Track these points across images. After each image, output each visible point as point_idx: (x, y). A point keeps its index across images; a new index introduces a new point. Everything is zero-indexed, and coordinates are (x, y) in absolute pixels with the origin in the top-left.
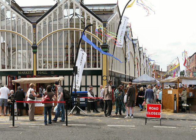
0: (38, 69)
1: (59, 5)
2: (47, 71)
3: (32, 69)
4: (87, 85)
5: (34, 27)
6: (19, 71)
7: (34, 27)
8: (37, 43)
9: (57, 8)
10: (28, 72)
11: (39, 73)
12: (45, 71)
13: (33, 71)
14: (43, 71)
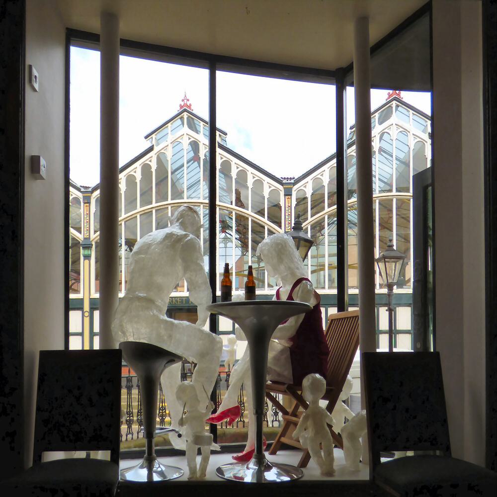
1: (156, 149)
5: (288, 194)
7: (288, 194)
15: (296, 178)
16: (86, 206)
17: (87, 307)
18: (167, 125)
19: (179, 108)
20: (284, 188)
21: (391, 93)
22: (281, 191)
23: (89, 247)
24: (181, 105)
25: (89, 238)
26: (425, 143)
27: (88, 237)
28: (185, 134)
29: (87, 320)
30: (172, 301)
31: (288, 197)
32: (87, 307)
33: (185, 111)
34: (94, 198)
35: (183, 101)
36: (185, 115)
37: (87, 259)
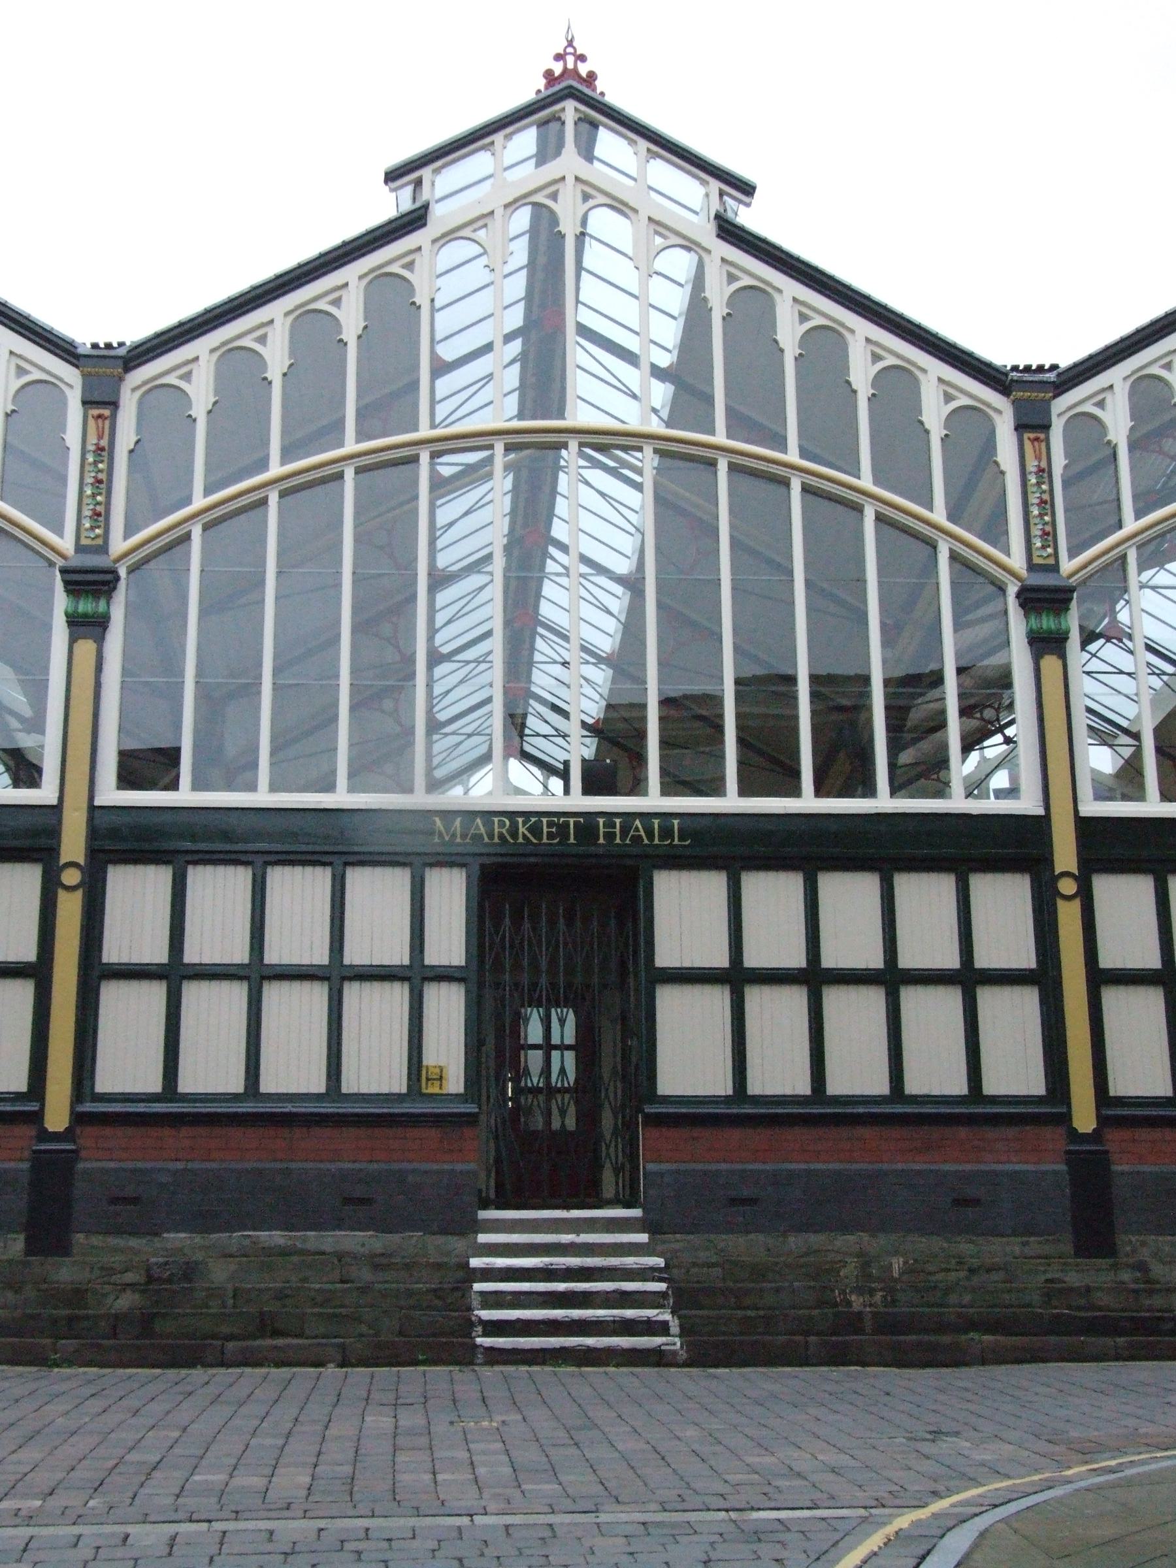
3: (45, 794)
4: (978, 964)
10: (488, 824)
11: (610, 836)
15: (128, 344)
17: (1065, 856)
19: (541, 83)
20: (83, 375)
21: (557, 73)
22: (71, 386)
23: (104, 583)
24: (549, 74)
25: (103, 549)
26: (704, 255)
27: (100, 542)
28: (570, 180)
29: (70, 908)
30: (514, 832)
31: (96, 412)
32: (1065, 856)
33: (571, 94)
34: (134, 390)
35: (559, 57)
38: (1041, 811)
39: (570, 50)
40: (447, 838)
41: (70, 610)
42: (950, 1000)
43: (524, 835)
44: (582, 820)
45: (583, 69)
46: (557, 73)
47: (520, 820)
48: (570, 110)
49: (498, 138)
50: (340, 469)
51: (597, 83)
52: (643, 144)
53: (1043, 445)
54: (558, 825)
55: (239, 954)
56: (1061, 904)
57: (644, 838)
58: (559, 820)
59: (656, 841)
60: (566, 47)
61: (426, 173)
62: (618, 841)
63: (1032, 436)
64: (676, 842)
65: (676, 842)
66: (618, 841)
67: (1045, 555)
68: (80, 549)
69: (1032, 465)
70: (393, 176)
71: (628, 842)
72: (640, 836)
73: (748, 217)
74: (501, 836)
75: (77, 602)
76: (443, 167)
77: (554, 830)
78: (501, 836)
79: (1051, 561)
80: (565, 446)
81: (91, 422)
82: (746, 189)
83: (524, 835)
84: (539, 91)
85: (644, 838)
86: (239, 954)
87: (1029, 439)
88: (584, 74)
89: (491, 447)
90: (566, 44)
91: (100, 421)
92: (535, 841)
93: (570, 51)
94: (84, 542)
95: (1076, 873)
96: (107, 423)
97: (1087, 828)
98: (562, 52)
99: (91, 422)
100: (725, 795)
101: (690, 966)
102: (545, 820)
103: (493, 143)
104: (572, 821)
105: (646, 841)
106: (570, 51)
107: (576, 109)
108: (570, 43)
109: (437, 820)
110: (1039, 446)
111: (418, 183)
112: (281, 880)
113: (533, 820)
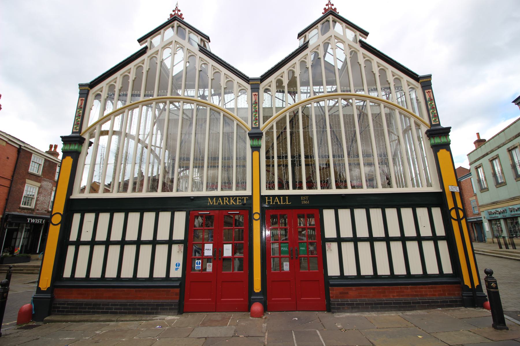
0: (265, 192)
2: (291, 197)
3: (248, 192)
4: (390, 236)
6: (212, 198)
8: (262, 126)
9: (145, 57)
10: (235, 200)
12: (284, 196)
13: (250, 198)
14: (279, 196)
16: (427, 92)
18: (316, 26)
21: (327, 9)
24: (325, 9)
25: (259, 128)
35: (174, 11)
36: (176, 23)
37: (256, 150)
38: (441, 191)
39: (329, 3)
40: (211, 204)
41: (252, 144)
42: (351, 245)
43: (232, 203)
44: (248, 198)
45: (333, 8)
46: (327, 9)
47: (231, 198)
48: (331, 17)
49: (162, 31)
50: (124, 110)
51: (337, 10)
52: (344, 24)
53: (431, 93)
54: (241, 200)
55: (167, 238)
56: (254, 221)
57: (278, 202)
58: (241, 198)
59: (282, 203)
60: (176, 8)
61: (307, 33)
62: (271, 203)
63: (427, 91)
64: (287, 203)
65: (287, 203)
66: (271, 203)
67: (256, 125)
68: (252, 128)
69: (428, 97)
70: (300, 35)
71: (217, 204)
72: (277, 202)
73: (368, 41)
74: (226, 203)
75: (253, 142)
76: (310, 32)
77: (240, 201)
78: (226, 203)
79: (438, 123)
80: (152, 103)
81: (253, 96)
82: (366, 34)
83: (232, 203)
84: (168, 19)
85: (278, 202)
86: (167, 238)
87: (426, 92)
88: (333, 8)
89: (338, 99)
90: (328, 2)
91: (255, 96)
92: (235, 204)
93: (177, 9)
94: (253, 126)
95: (62, 214)
96: (257, 96)
97: (263, 198)
98: (175, 10)
99: (253, 96)
100: (98, 193)
101: (379, 237)
102: (238, 198)
103: (318, 26)
104: (245, 198)
105: (279, 203)
106: (177, 9)
107: (332, 17)
108: (329, 2)
109: (209, 199)
110: (83, 101)
111: (305, 37)
112: (341, 212)
113: (235, 198)
